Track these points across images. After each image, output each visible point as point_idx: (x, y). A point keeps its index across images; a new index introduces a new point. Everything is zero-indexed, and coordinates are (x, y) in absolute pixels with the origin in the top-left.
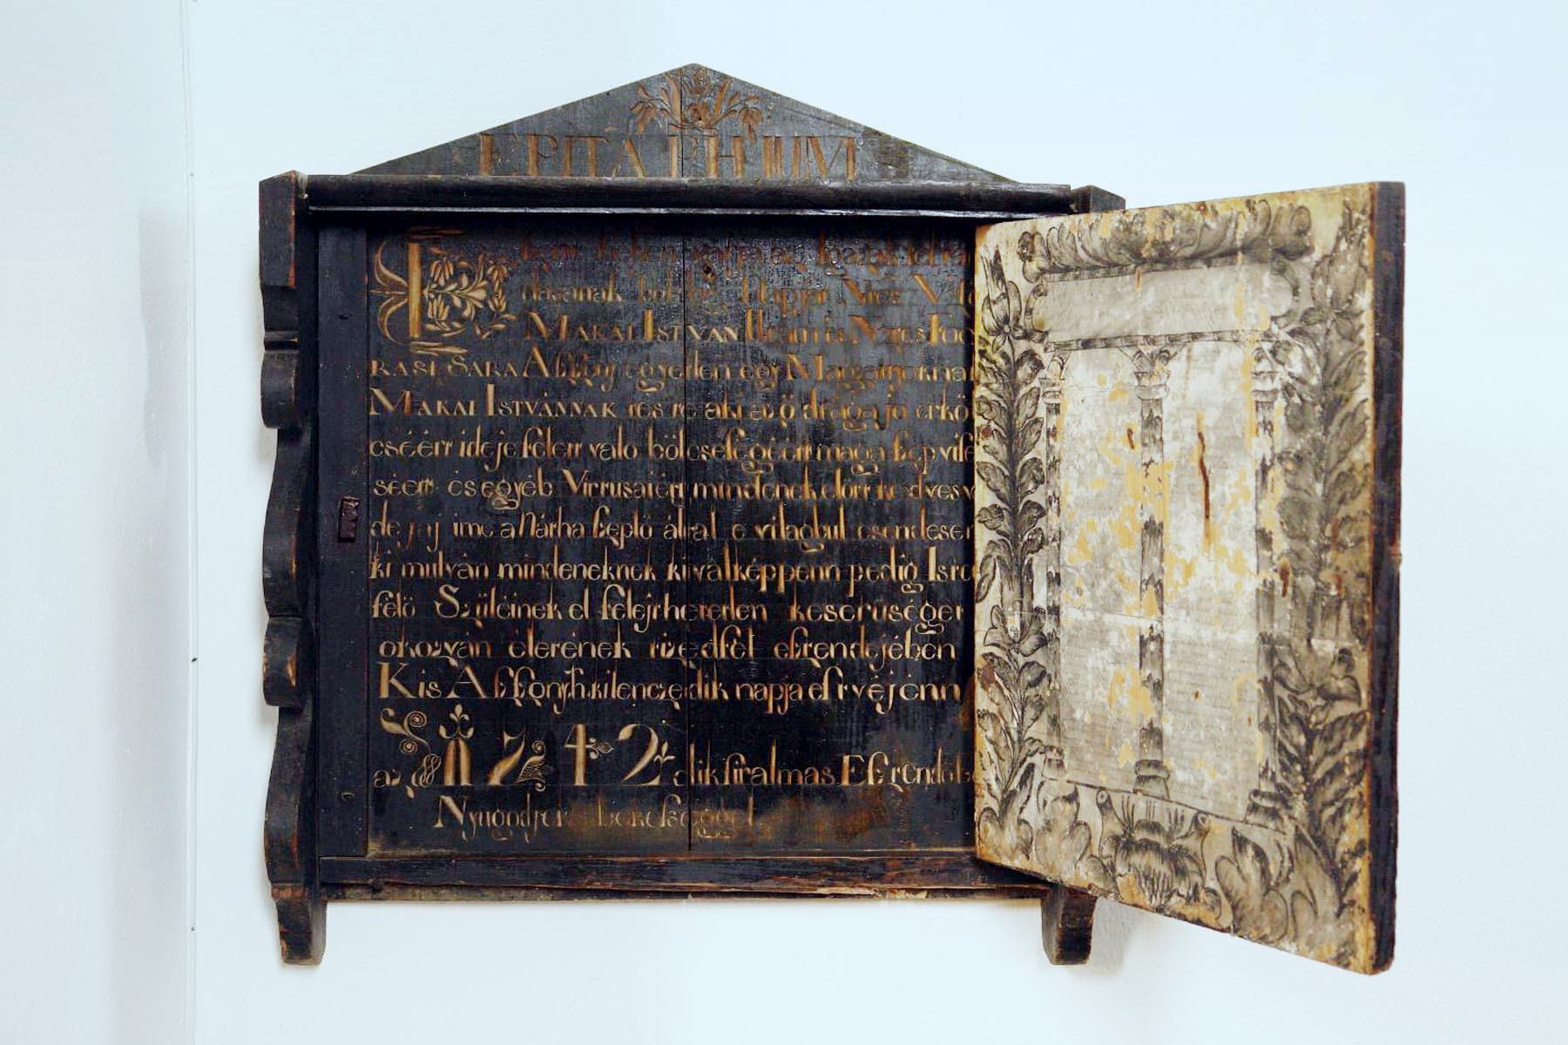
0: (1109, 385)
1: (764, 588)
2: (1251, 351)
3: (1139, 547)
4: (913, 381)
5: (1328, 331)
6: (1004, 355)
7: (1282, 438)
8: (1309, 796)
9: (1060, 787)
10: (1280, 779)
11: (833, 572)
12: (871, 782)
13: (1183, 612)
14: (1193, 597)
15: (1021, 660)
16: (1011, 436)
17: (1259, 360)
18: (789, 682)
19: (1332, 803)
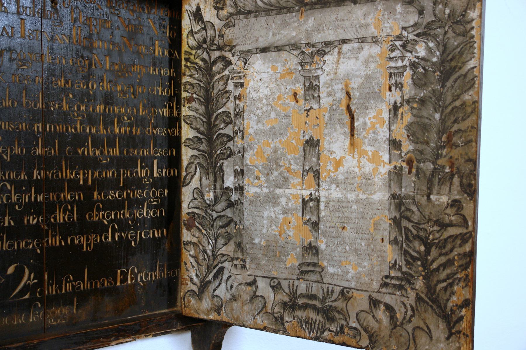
0: (280, 70)
1: (81, 183)
2: (386, 46)
3: (302, 153)
4: (148, 74)
5: (446, 33)
6: (203, 60)
7: (409, 90)
8: (427, 278)
9: (243, 279)
10: (404, 269)
11: (113, 173)
12: (129, 282)
13: (334, 186)
14: (341, 177)
15: (215, 215)
16: (209, 101)
17: (392, 51)
18: (94, 233)
19: (444, 281)
